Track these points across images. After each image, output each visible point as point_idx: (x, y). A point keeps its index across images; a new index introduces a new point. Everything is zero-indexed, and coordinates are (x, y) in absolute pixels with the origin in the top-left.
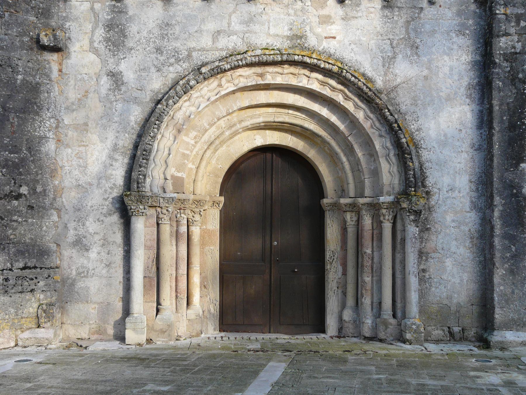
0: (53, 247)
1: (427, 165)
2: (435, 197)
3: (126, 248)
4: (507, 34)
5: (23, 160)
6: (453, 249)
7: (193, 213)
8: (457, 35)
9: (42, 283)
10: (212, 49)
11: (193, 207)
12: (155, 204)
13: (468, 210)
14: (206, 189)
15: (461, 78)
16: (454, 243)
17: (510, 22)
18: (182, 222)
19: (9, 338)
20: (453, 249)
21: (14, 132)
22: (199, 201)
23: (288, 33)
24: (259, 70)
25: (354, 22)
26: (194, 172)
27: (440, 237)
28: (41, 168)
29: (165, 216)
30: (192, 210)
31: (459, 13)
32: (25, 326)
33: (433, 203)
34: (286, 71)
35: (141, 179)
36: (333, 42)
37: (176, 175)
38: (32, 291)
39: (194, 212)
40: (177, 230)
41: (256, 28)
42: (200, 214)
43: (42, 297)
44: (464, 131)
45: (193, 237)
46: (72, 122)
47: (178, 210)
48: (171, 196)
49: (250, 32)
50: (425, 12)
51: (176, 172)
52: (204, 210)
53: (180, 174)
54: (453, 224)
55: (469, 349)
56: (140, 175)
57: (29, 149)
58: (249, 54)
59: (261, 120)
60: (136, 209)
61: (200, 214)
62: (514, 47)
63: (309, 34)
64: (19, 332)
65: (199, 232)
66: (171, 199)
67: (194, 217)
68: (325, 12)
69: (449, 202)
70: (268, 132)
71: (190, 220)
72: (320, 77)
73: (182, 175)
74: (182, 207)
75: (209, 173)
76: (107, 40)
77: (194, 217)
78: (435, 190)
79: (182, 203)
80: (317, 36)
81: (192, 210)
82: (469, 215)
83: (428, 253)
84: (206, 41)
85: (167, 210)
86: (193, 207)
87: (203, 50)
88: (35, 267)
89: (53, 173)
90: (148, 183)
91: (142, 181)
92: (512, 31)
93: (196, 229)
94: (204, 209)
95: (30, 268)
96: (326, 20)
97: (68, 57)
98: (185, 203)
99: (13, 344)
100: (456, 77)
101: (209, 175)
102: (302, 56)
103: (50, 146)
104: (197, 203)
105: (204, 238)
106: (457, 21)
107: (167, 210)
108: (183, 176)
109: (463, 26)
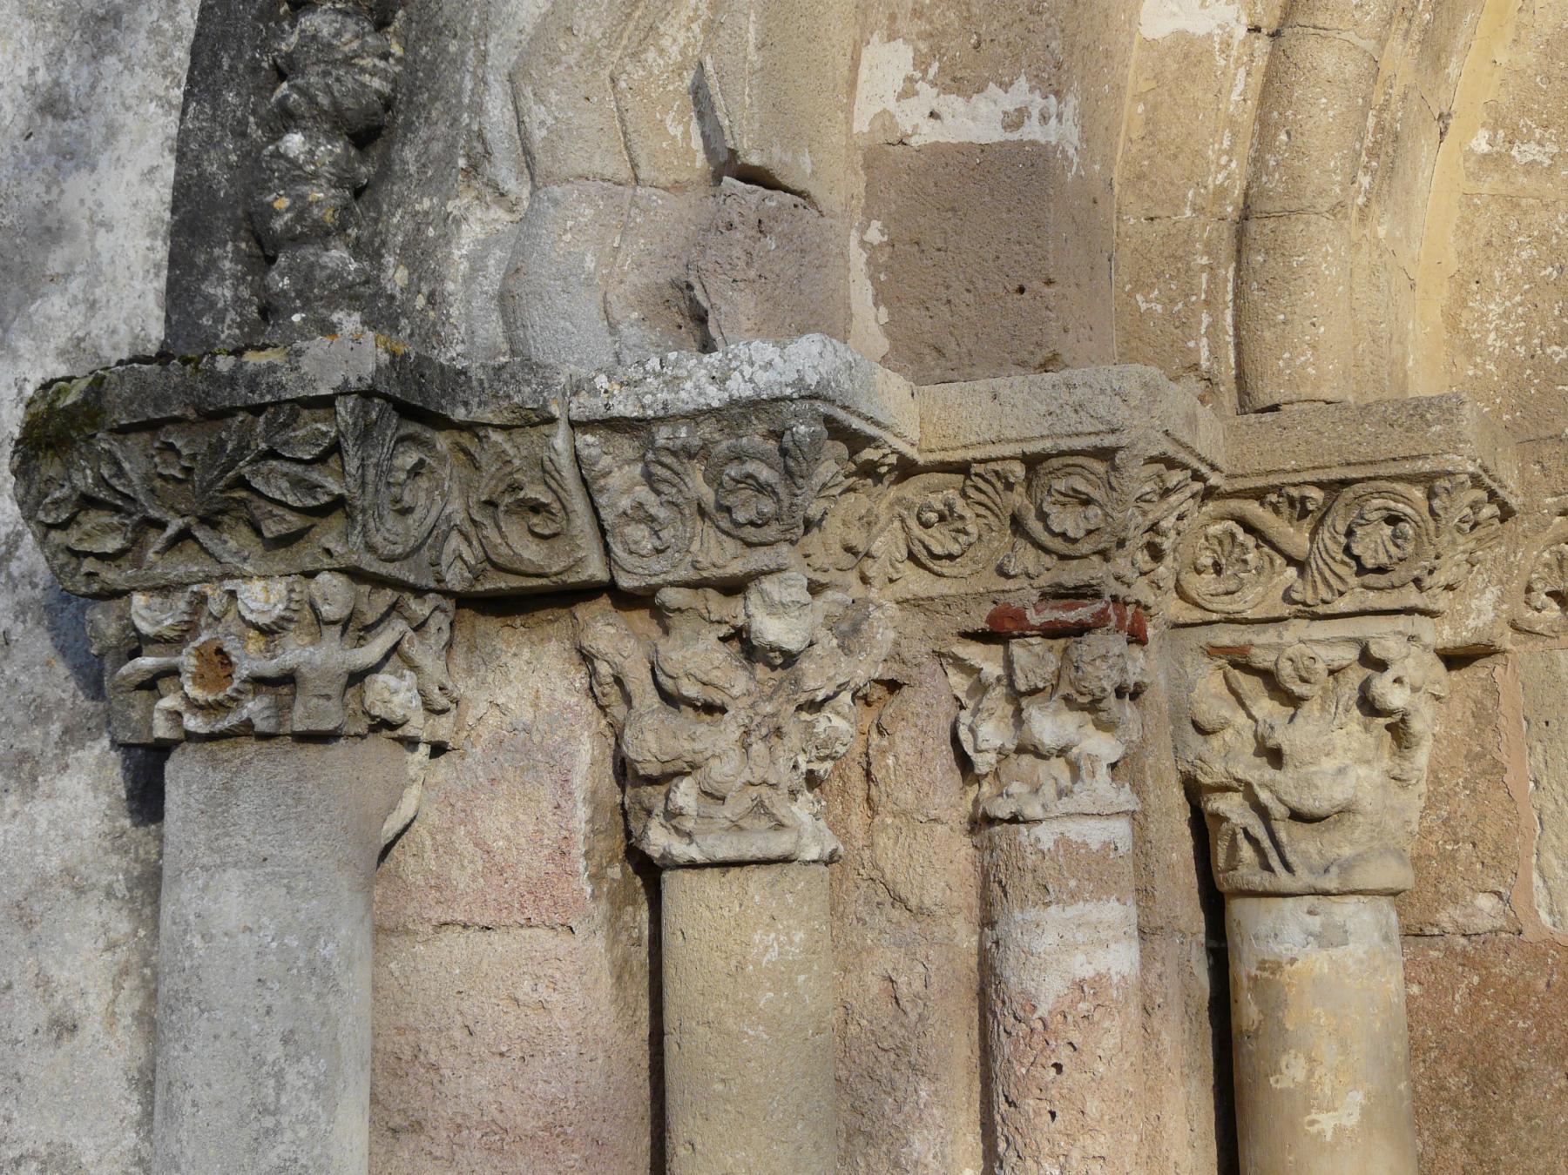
3: (1214, 944)
7: (1266, 707)
11: (1250, 602)
12: (532, 553)
14: (1470, 350)
18: (1046, 835)
22: (1334, 487)
26: (1240, 91)
29: (717, 739)
30: (1240, 661)
35: (295, 175)
37: (929, 134)
39: (1269, 677)
40: (983, 953)
42: (1369, 706)
45: (1292, 1072)
46: (526, 182)
47: (973, 653)
48: (739, 387)
51: (928, 96)
52: (1455, 659)
53: (982, 104)
55: (1308, 686)
56: (286, 119)
60: (188, 630)
61: (1369, 706)
65: (1392, 983)
66: (754, 438)
67: (1275, 757)
71: (1230, 806)
73: (1015, 120)
74: (1023, 595)
75: (1496, 121)
77: (1275, 757)
79: (1017, 524)
81: (1240, 661)
85: (742, 641)
86: (1258, 597)
90: (477, 263)
91: (301, 210)
93: (1329, 938)
94: (1446, 635)
98: (1068, 520)
101: (1495, 161)
104: (1296, 538)
105: (1484, 1083)
107: (742, 641)
108: (1032, 131)
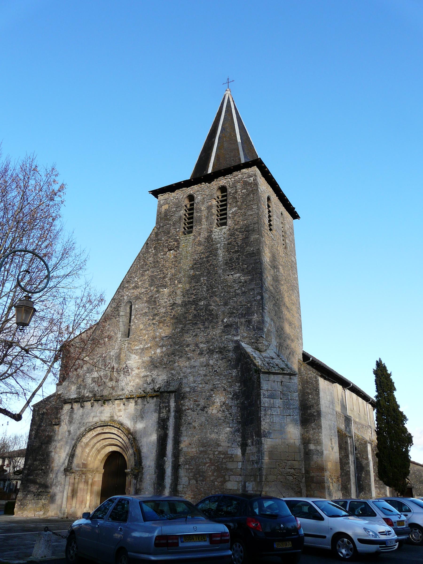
0: (50, 485)
1: (143, 458)
2: (144, 470)
4: (163, 413)
5: (44, 458)
6: (148, 488)
8: (154, 413)
9: (44, 497)
10: (92, 422)
13: (154, 474)
15: (154, 427)
16: (149, 486)
17: (164, 409)
19: (33, 514)
20: (148, 488)
21: (43, 450)
23: (110, 416)
24: (102, 428)
25: (127, 411)
27: (145, 484)
28: (49, 461)
31: (155, 405)
32: (37, 510)
33: (143, 471)
34: (108, 428)
36: (121, 418)
38: (41, 499)
41: (102, 415)
43: (43, 501)
44: (154, 446)
49: (101, 416)
50: (146, 405)
54: (149, 479)
57: (47, 455)
58: (98, 423)
59: (107, 443)
62: (164, 417)
63: (115, 416)
64: (36, 512)
68: (120, 408)
69: (148, 471)
70: (113, 446)
72: (117, 429)
76: (69, 421)
78: (144, 467)
80: (117, 416)
82: (154, 476)
83: (141, 490)
84: (91, 420)
87: (90, 422)
88: (43, 492)
89: (52, 462)
92: (164, 411)
95: (42, 492)
96: (120, 410)
97: (60, 426)
99: (33, 516)
100: (153, 427)
102: (290, 382)
103: (53, 454)
106: (155, 408)
109: (156, 409)
